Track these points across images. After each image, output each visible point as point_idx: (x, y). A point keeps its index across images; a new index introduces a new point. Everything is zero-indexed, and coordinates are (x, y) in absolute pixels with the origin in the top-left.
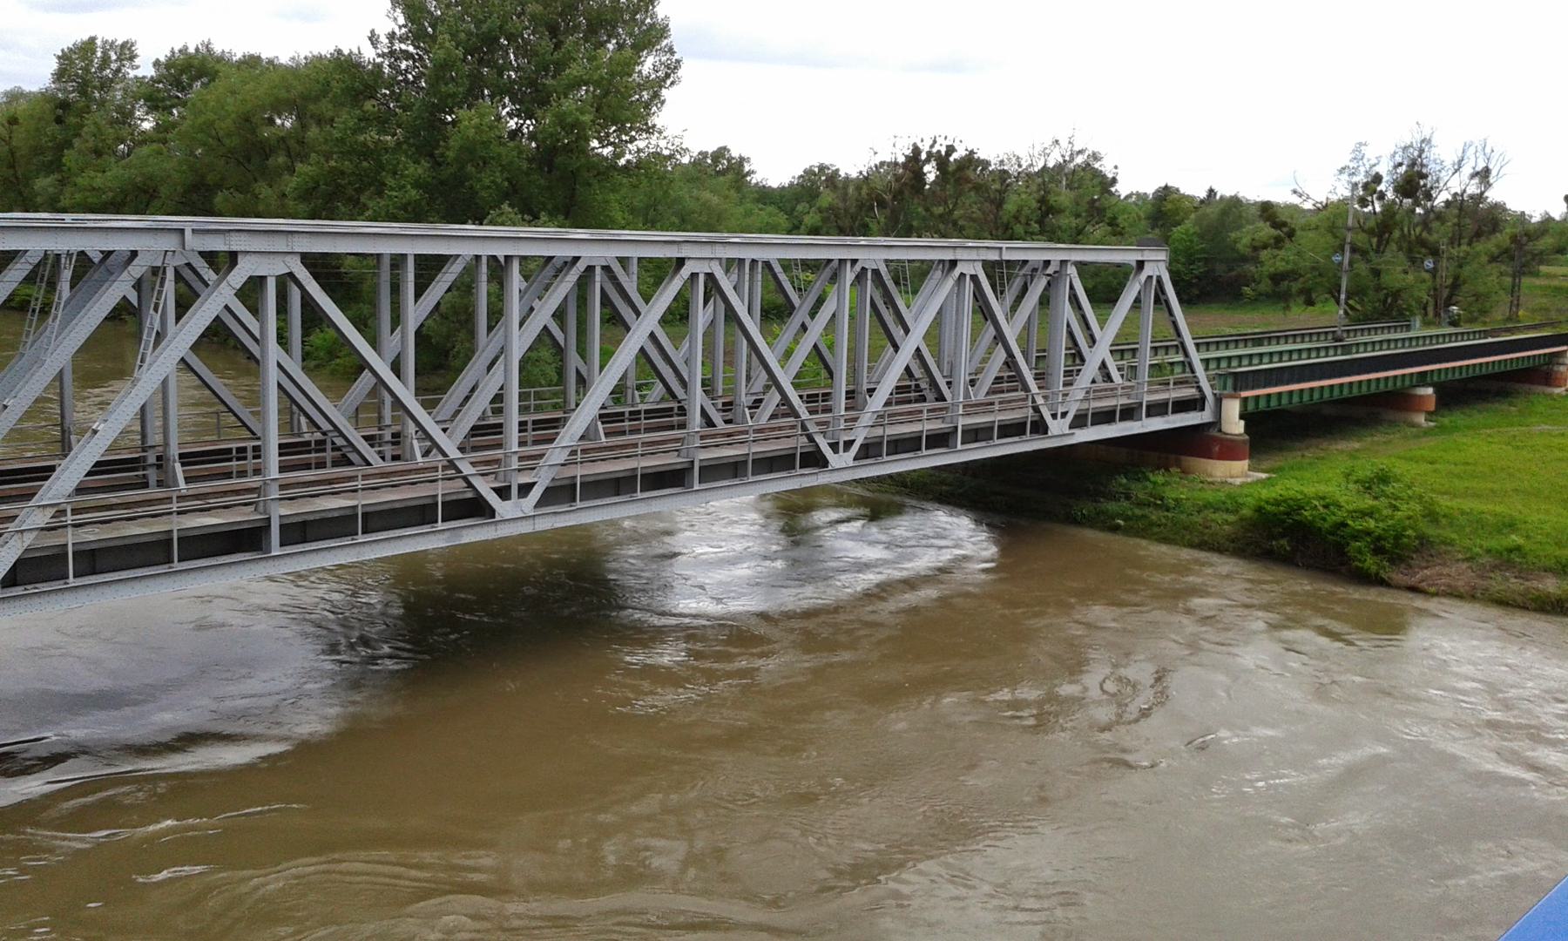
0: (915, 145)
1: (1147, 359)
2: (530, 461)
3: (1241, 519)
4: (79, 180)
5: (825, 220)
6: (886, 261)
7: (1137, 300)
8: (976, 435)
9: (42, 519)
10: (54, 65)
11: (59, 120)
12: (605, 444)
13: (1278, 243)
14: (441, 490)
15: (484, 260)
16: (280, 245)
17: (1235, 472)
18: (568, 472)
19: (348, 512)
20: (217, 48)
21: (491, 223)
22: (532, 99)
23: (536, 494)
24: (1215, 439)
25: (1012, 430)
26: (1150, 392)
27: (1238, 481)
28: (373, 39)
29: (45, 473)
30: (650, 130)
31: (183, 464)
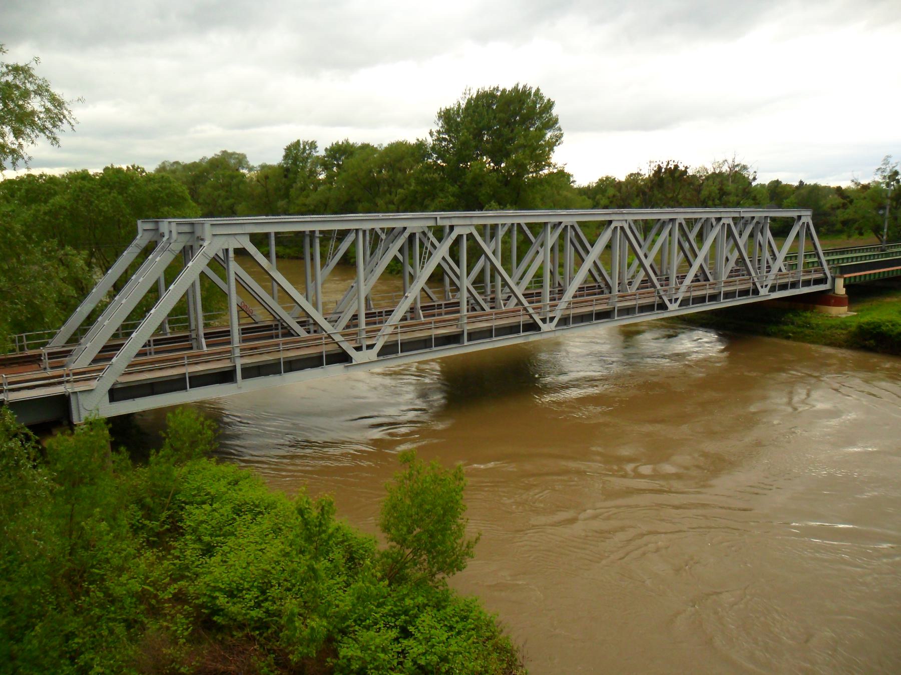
0: (659, 165)
1: (801, 261)
2: (372, 334)
3: (849, 332)
4: (297, 202)
5: (611, 202)
6: (685, 219)
7: (798, 235)
8: (729, 295)
9: (390, 330)
10: (283, 153)
11: (286, 176)
12: (206, 352)
13: (844, 206)
14: (324, 349)
15: (515, 225)
16: (468, 222)
17: (841, 312)
18: (568, 312)
19: (276, 361)
20: (351, 142)
21: (486, 210)
22: (497, 155)
23: (556, 321)
24: (832, 297)
25: (744, 293)
26: (804, 275)
27: (844, 316)
28: (431, 134)
29: (389, 313)
30: (549, 165)
31: (205, 338)
